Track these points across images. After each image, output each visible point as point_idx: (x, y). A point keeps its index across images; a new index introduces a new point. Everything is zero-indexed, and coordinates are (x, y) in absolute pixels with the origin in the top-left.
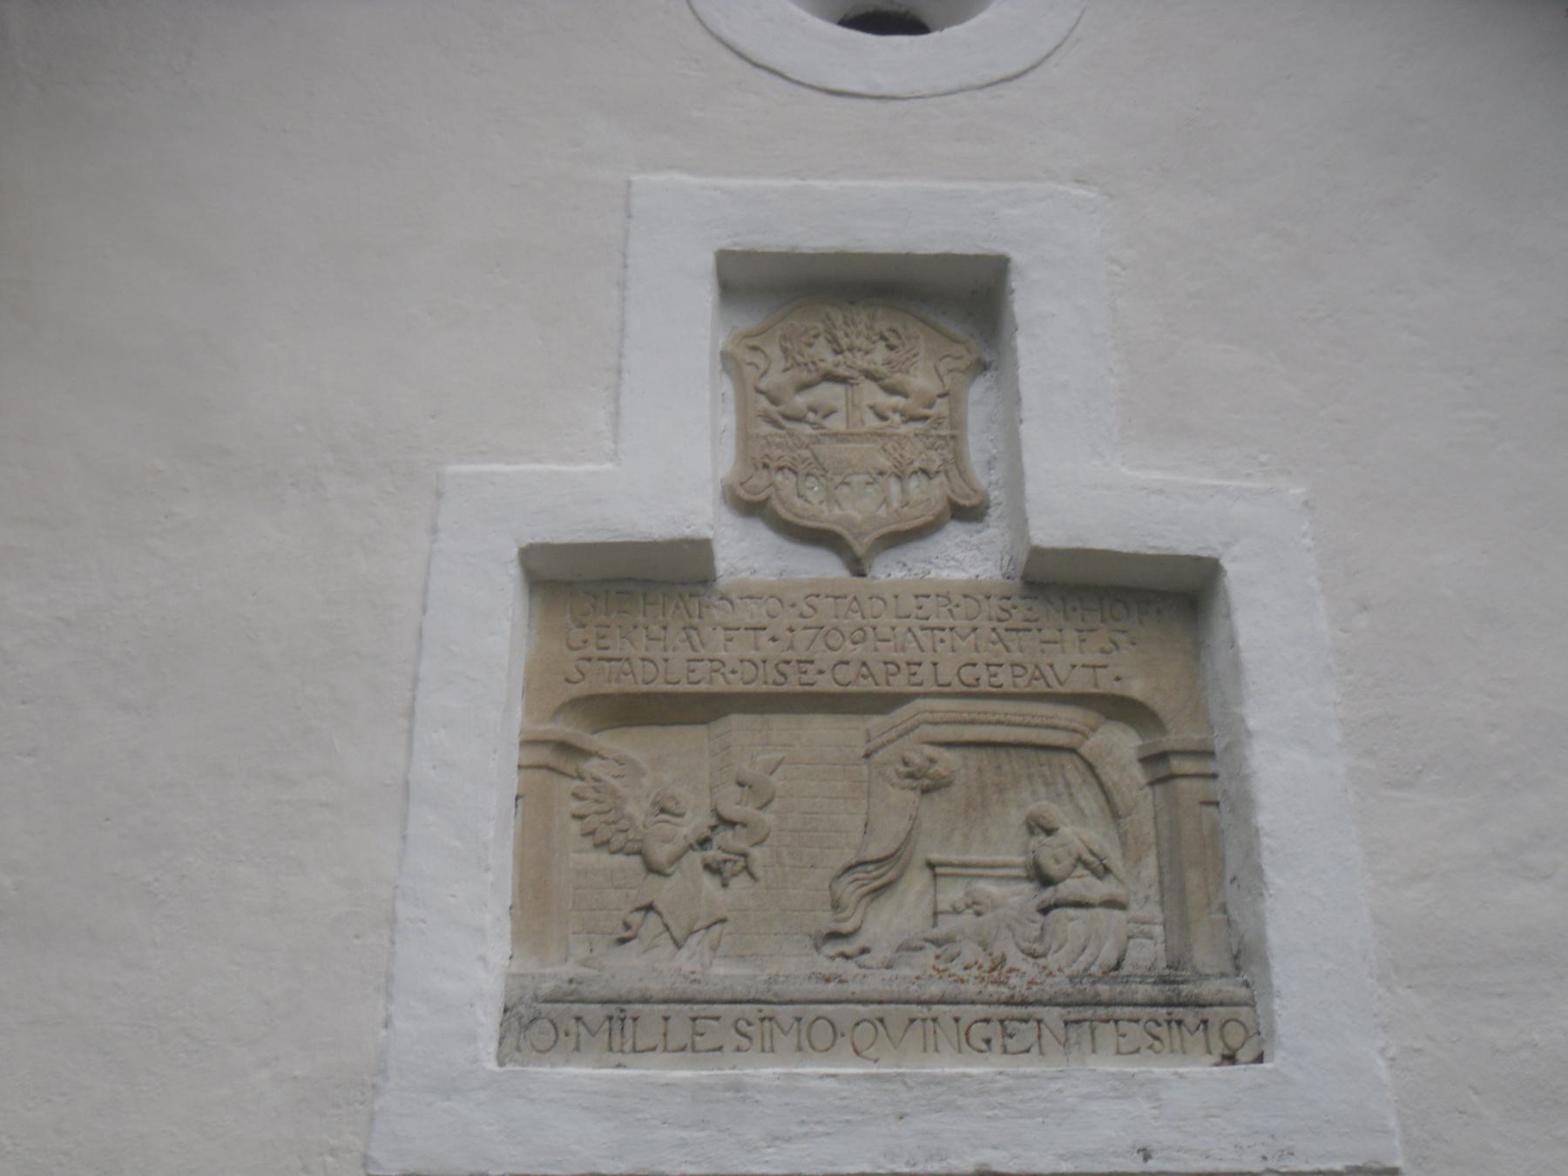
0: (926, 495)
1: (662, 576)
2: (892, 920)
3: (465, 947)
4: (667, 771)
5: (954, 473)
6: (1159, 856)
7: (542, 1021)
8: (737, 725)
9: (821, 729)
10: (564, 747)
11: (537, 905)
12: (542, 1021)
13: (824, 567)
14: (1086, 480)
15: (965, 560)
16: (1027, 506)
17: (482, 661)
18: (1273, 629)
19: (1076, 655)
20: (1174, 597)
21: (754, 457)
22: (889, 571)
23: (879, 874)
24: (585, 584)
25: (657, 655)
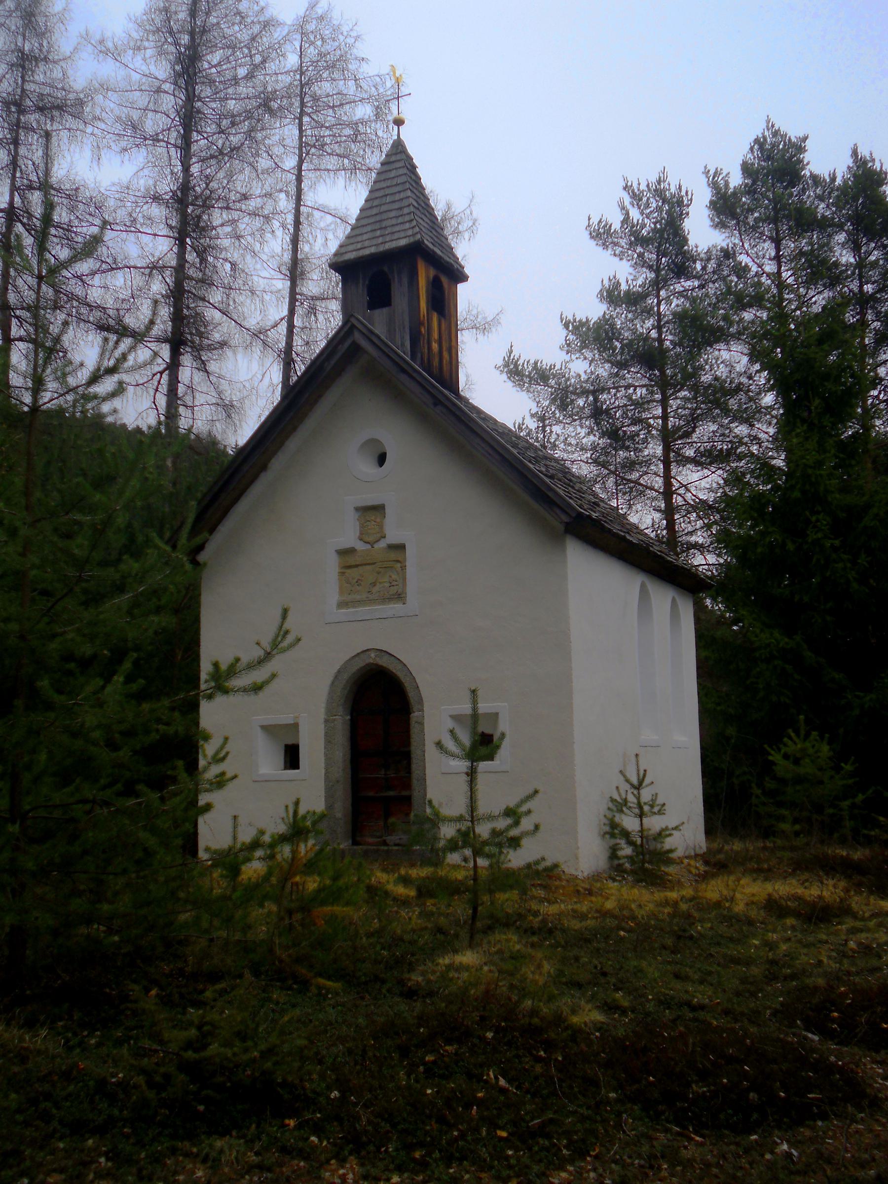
0: (379, 535)
1: (351, 551)
2: (375, 590)
3: (334, 597)
4: (354, 573)
5: (191, 95)
6: (603, 1023)
7: (342, 605)
8: (360, 568)
9: (368, 567)
10: (344, 573)
11: (341, 591)
12: (342, 605)
13: (369, 547)
14: (393, 535)
15: (382, 544)
16: (273, 461)
17: (333, 564)
18: (410, 552)
19: (393, 555)
20: (401, 547)
21: (361, 533)
22: (376, 546)
23: (374, 584)
24: (344, 553)
25: (351, 560)
